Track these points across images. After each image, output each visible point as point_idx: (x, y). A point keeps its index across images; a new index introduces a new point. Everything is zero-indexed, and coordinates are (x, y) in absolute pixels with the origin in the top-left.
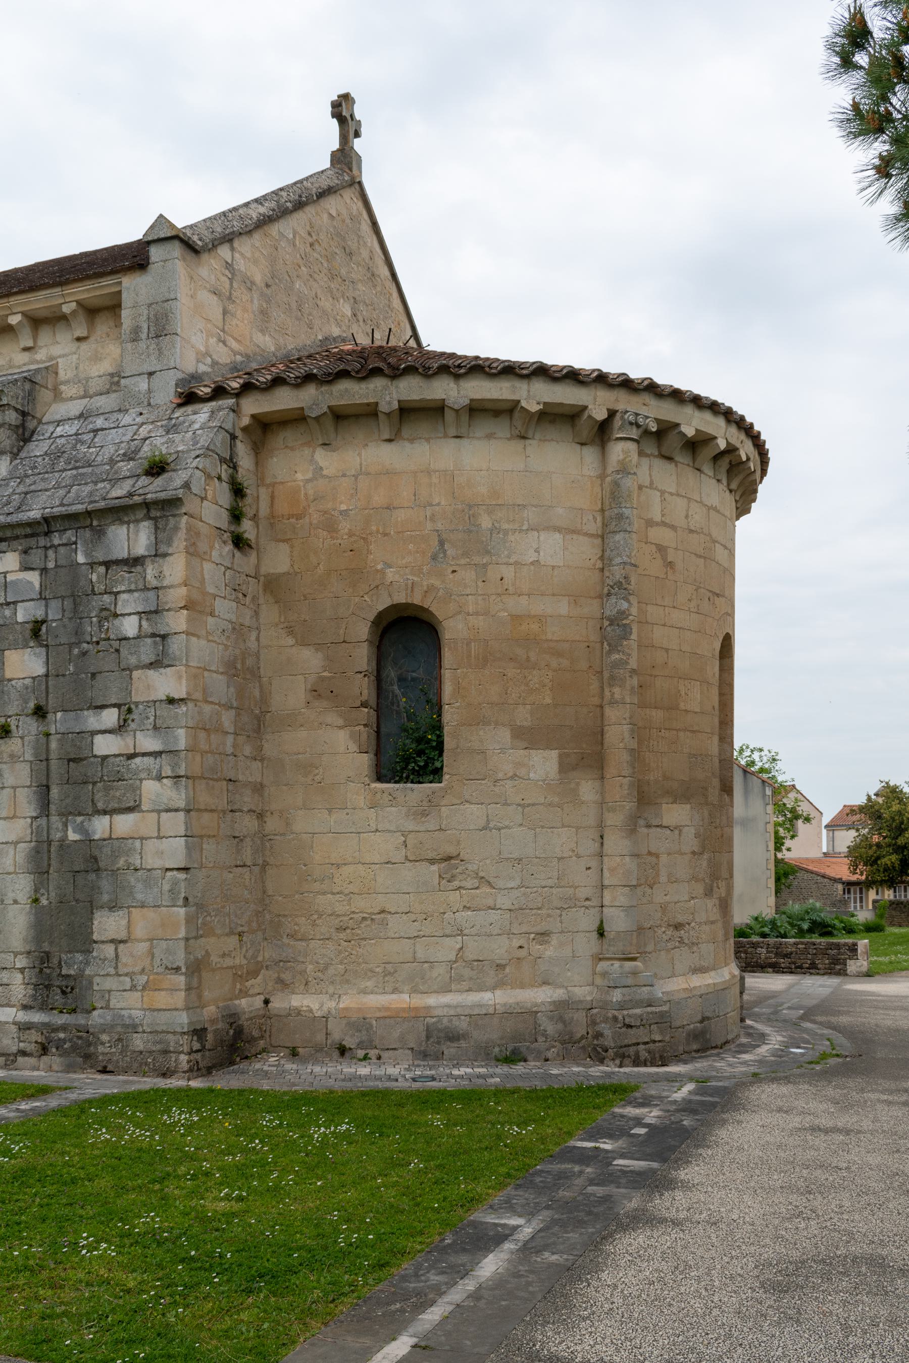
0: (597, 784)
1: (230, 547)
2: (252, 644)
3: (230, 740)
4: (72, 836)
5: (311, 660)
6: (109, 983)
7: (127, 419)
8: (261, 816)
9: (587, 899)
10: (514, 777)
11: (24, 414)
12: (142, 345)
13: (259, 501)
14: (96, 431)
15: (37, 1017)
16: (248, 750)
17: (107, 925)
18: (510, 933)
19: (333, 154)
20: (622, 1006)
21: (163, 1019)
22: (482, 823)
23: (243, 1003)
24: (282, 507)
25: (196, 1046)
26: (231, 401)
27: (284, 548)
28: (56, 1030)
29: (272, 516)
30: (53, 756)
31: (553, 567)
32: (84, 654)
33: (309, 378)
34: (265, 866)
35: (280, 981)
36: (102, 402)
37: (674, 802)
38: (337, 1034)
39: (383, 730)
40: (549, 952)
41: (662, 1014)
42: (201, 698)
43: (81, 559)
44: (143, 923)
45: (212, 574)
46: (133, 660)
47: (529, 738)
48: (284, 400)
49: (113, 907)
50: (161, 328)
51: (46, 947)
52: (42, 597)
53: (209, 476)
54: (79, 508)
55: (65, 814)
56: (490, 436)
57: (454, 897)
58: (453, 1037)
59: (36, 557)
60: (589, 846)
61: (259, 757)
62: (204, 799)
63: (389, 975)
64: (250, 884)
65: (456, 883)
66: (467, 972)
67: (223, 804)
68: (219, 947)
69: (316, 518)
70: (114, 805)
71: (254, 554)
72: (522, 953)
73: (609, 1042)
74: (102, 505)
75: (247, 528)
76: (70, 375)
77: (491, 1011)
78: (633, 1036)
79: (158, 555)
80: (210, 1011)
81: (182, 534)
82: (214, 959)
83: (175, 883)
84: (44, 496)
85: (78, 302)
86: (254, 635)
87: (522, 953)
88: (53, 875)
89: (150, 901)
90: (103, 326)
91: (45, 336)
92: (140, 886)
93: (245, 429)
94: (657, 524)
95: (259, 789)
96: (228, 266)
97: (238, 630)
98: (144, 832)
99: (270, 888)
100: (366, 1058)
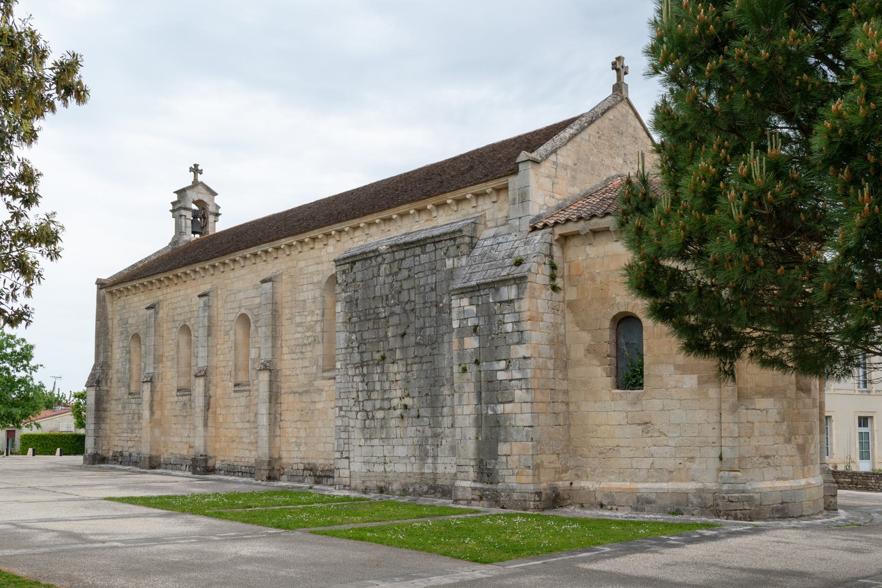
0: (718, 390)
1: (550, 291)
2: (562, 330)
3: (551, 372)
4: (490, 412)
5: (586, 337)
6: (504, 472)
7: (510, 238)
8: (567, 404)
10: (676, 387)
11: (472, 237)
12: (516, 206)
13: (563, 268)
14: (499, 244)
15: (478, 485)
16: (560, 376)
17: (503, 448)
18: (675, 457)
19: (614, 86)
20: (727, 492)
21: (524, 487)
22: (661, 407)
23: (560, 483)
24: (573, 272)
25: (537, 499)
26: (550, 230)
27: (574, 289)
28: (485, 490)
29: (570, 276)
30: (482, 380)
32: (493, 339)
33: (580, 218)
34: (569, 425)
35: (577, 475)
36: (503, 230)
37: (763, 397)
38: (600, 498)
39: (619, 366)
40: (695, 466)
41: (750, 497)
43: (491, 300)
44: (516, 448)
45: (541, 304)
46: (511, 342)
48: (571, 228)
49: (505, 441)
50: (524, 198)
51: (481, 457)
52: (477, 316)
53: (539, 264)
54: (490, 280)
55: (487, 403)
57: (649, 440)
58: (649, 502)
59: (474, 300)
60: (714, 418)
61: (565, 378)
62: (539, 397)
63: (621, 474)
64: (566, 434)
65: (650, 434)
66: (655, 474)
67: (549, 399)
68: (548, 459)
69: (587, 276)
70: (505, 400)
71: (562, 292)
72: (681, 466)
73: (721, 508)
74: (498, 279)
75: (559, 282)
76: (491, 217)
78: (733, 506)
79: (519, 299)
80: (544, 485)
81: (528, 290)
82: (545, 464)
83: (528, 432)
84: (477, 275)
85: (493, 188)
86: (563, 327)
87: (681, 466)
88: (483, 428)
89: (519, 439)
90: (502, 196)
91: (481, 201)
92: (515, 433)
93: (557, 240)
95: (566, 392)
96: (555, 163)
97: (555, 326)
98: (516, 411)
99: (572, 434)
100: (611, 509)
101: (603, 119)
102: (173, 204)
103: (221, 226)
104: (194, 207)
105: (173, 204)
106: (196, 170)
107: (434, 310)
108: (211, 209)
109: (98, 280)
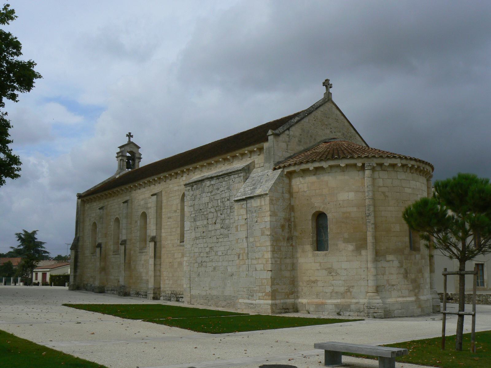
9: (364, 278)
31: (352, 200)
42: (418, 195)
47: (347, 241)
48: (292, 169)
56: (336, 172)
77: (340, 304)
94: (381, 187)
101: (317, 111)
102: (117, 153)
103: (143, 163)
104: (128, 155)
105: (117, 153)
106: (130, 136)
107: (229, 210)
108: (137, 156)
109: (78, 194)
